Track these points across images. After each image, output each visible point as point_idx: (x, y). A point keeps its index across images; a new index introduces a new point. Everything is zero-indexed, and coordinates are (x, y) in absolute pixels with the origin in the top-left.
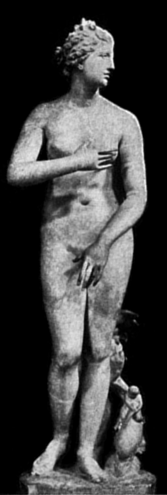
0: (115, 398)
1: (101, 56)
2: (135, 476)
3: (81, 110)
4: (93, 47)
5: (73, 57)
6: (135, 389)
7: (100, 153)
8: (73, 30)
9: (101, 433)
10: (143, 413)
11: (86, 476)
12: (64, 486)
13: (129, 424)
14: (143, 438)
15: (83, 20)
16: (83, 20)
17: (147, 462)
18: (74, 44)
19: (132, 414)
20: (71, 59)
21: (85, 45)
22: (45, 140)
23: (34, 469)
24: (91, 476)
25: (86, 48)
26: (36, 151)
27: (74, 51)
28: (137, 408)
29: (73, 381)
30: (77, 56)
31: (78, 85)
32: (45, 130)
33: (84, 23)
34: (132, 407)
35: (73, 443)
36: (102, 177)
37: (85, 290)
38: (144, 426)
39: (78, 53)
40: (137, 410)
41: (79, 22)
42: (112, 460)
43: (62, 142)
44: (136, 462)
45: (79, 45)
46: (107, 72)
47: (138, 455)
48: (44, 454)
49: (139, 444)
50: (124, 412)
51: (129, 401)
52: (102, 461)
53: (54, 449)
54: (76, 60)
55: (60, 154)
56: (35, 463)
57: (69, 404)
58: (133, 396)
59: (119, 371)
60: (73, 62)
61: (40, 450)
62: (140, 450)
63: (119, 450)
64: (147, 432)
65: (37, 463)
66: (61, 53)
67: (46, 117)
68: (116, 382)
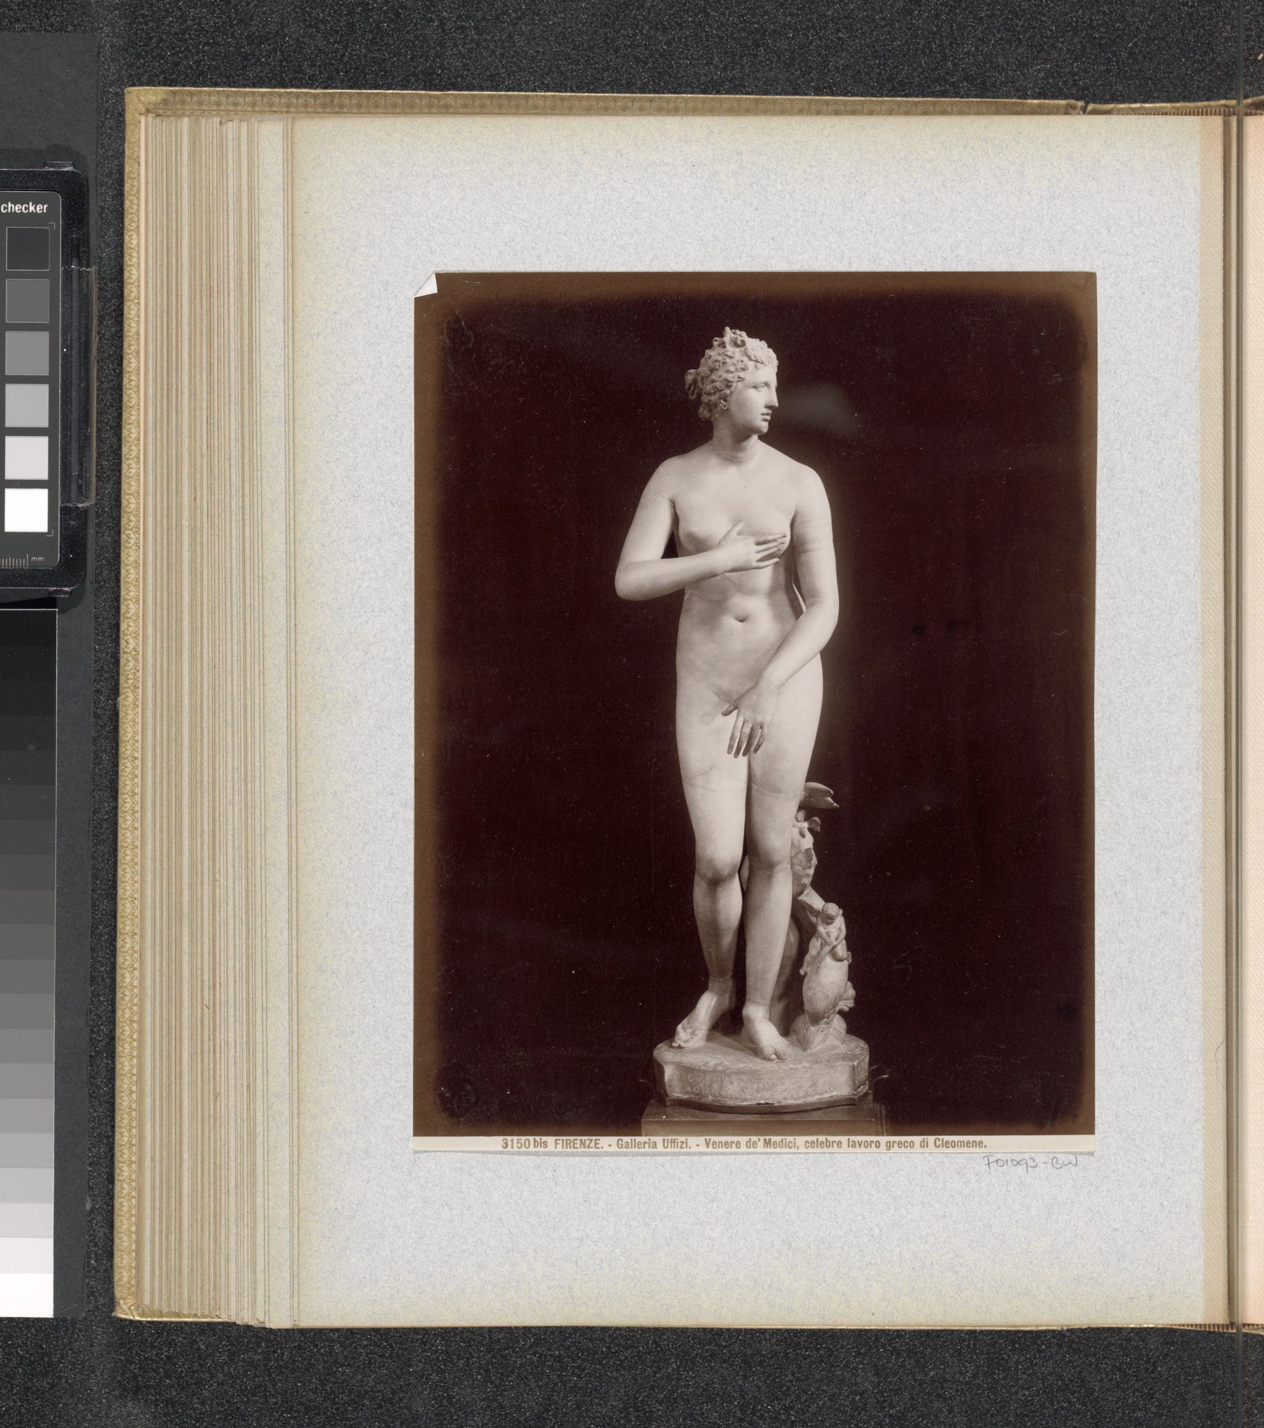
0: (803, 924)
1: (755, 387)
2: (834, 1047)
3: (732, 471)
4: (742, 374)
5: (712, 391)
6: (833, 909)
7: (758, 544)
8: (710, 346)
9: (784, 979)
10: (850, 947)
11: (755, 1050)
12: (720, 1065)
13: (823, 964)
14: (849, 984)
15: (727, 329)
16: (727, 329)
17: (857, 1022)
18: (712, 370)
19: (827, 949)
20: (709, 394)
21: (728, 371)
22: (676, 520)
23: (677, 1038)
24: (762, 1049)
25: (730, 376)
26: (660, 548)
27: (713, 381)
28: (837, 939)
29: (731, 901)
30: (717, 390)
31: (722, 432)
32: (673, 504)
33: (729, 334)
34: (827, 938)
35: (740, 995)
36: (765, 577)
37: (743, 760)
38: (850, 966)
39: (718, 384)
40: (835, 943)
41: (721, 335)
42: (801, 1022)
43: (696, 525)
44: (839, 1024)
45: (721, 372)
46: (767, 411)
47: (841, 1013)
48: (693, 1015)
49: (840, 997)
50: (815, 945)
51: (821, 929)
52: (786, 1028)
53: (707, 1006)
54: (717, 396)
55: (700, 546)
56: (680, 1027)
57: (728, 940)
58: (829, 920)
59: (807, 881)
60: (713, 398)
61: (687, 1007)
62: (847, 1005)
63: (807, 1006)
64: (855, 975)
65: (684, 1029)
66: (695, 382)
67: (716, 372)
68: (802, 898)
